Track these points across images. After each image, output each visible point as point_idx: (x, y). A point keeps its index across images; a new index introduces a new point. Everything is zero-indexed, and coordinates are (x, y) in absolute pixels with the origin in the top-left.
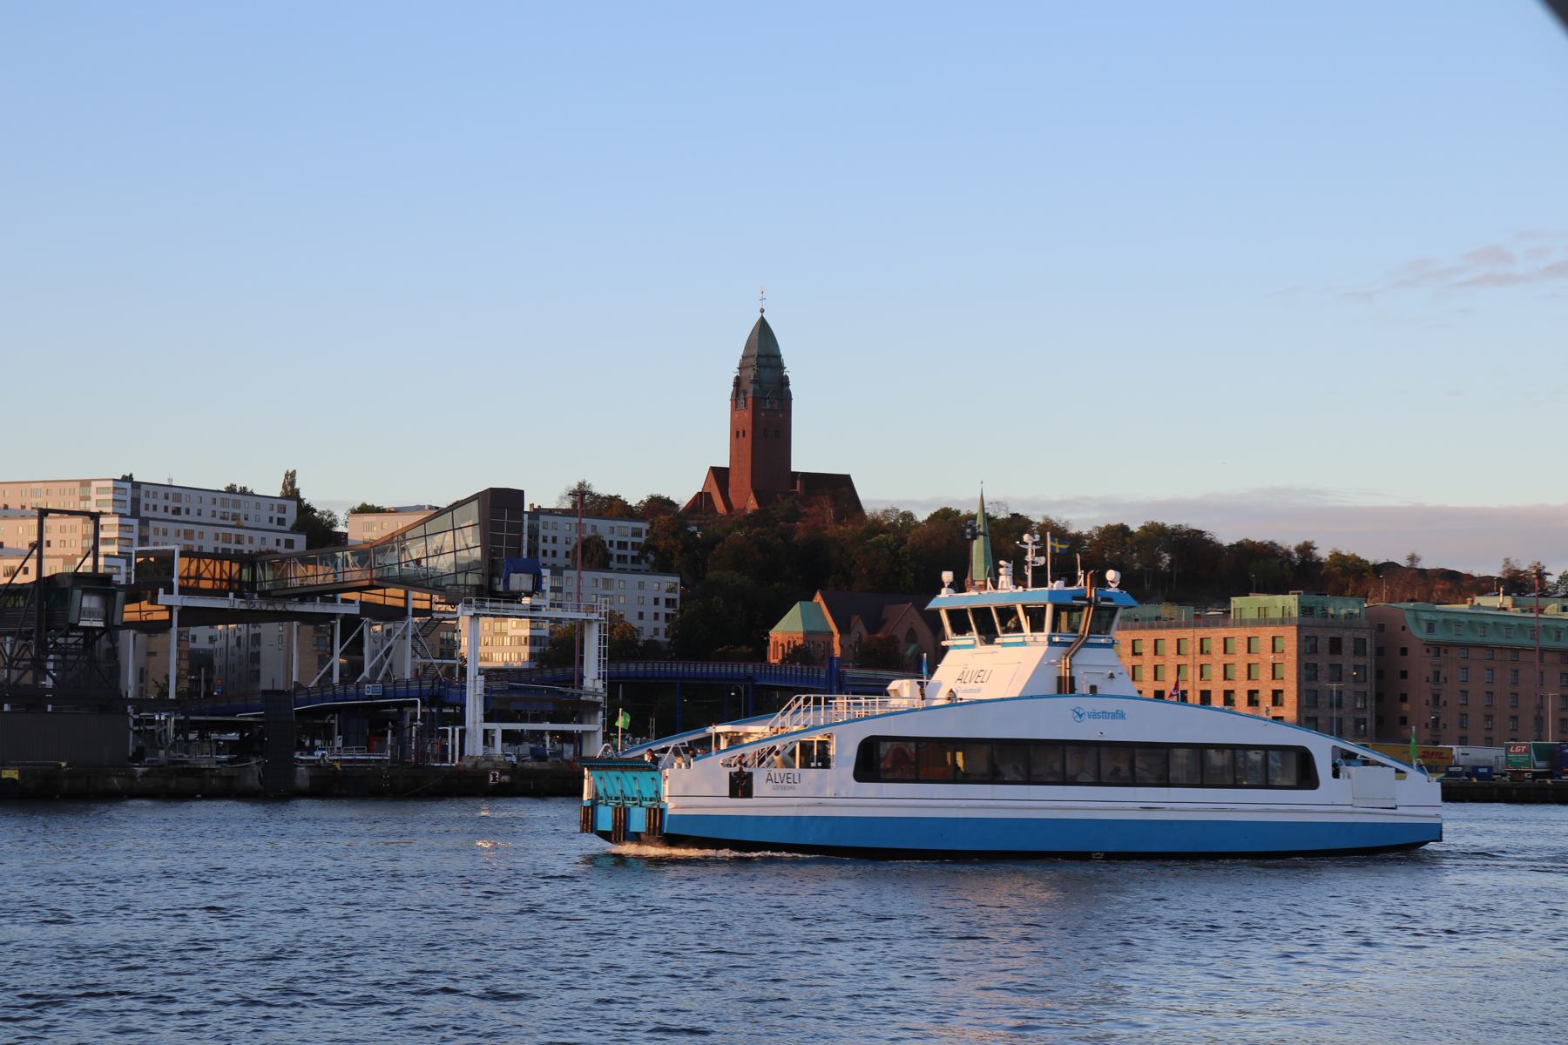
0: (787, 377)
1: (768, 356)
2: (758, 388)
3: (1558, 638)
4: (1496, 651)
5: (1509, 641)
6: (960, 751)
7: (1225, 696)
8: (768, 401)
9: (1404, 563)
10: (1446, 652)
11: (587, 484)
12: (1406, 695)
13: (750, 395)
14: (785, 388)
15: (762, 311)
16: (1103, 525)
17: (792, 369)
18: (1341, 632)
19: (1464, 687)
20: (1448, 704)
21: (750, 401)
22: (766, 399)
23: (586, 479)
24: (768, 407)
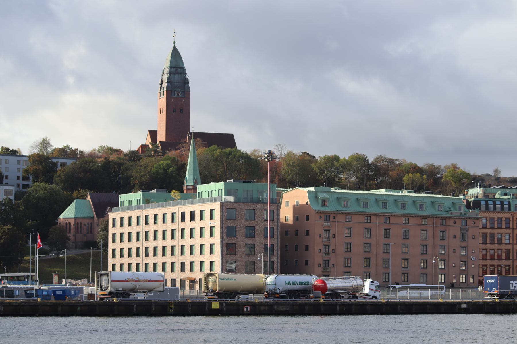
0: (187, 79)
1: (176, 68)
2: (170, 85)
3: (346, 206)
4: (372, 217)
5: (384, 211)
6: (467, 306)
7: (120, 250)
8: (175, 92)
9: (492, 173)
10: (334, 218)
11: (47, 139)
12: (308, 246)
13: (165, 89)
14: (187, 85)
15: (175, 43)
16: (109, 146)
17: (190, 76)
18: (254, 206)
19: (348, 240)
20: (336, 251)
21: (165, 92)
22: (174, 91)
23: (47, 137)
24: (176, 96)
